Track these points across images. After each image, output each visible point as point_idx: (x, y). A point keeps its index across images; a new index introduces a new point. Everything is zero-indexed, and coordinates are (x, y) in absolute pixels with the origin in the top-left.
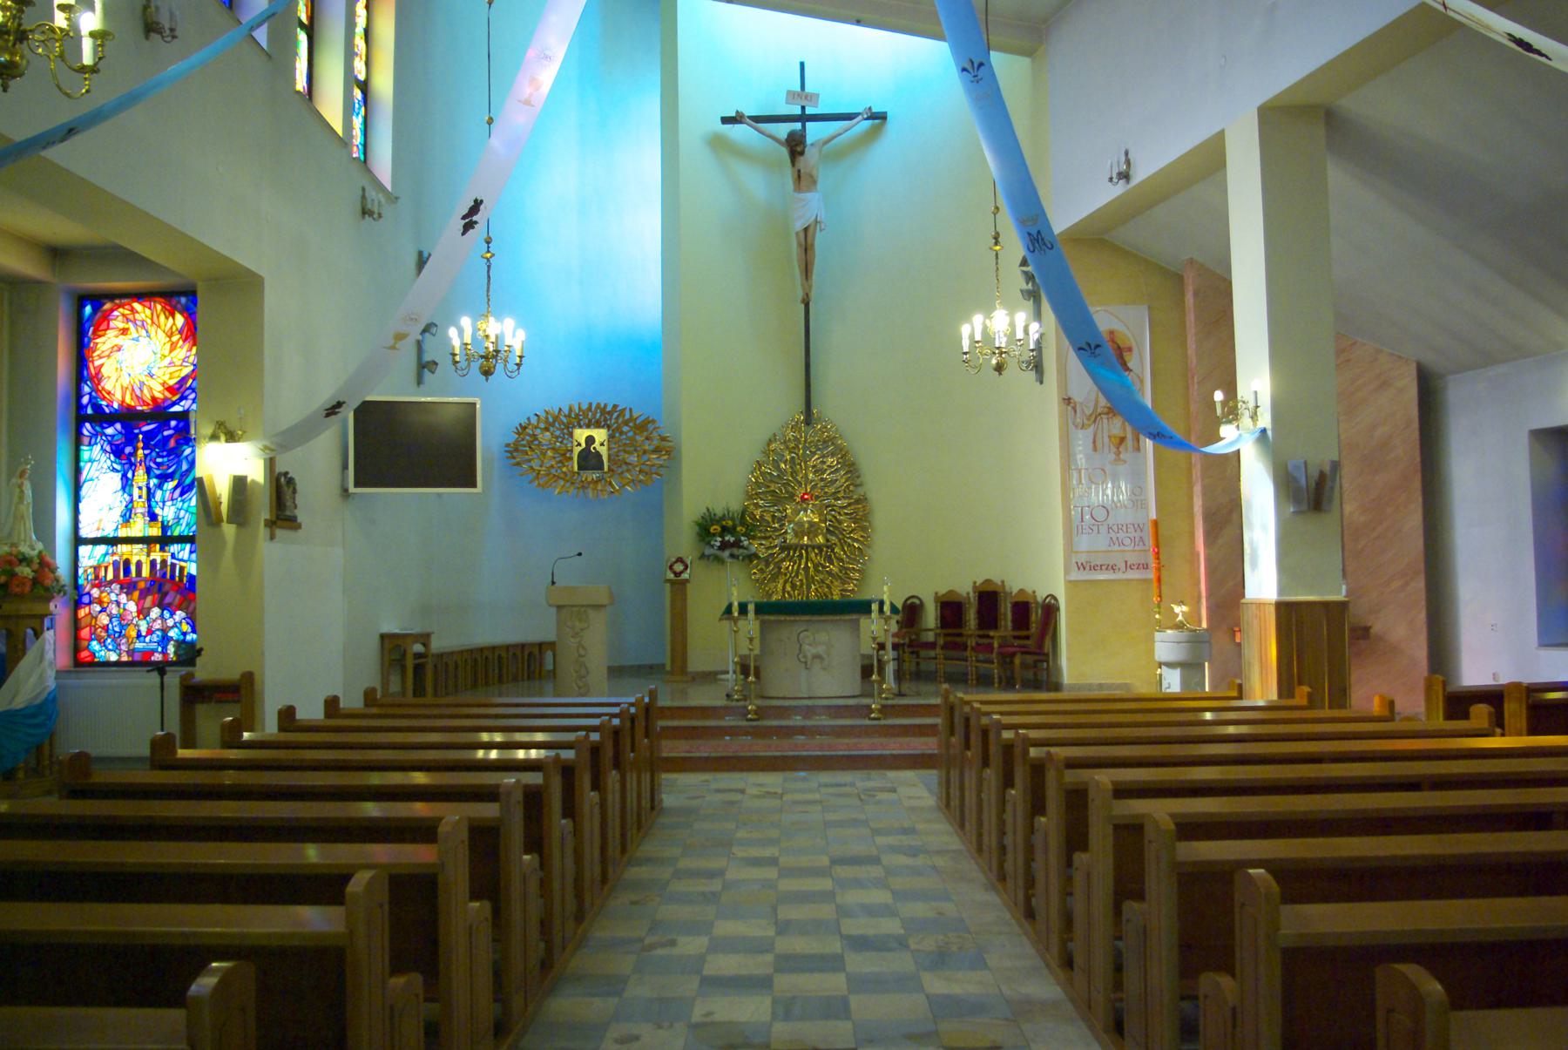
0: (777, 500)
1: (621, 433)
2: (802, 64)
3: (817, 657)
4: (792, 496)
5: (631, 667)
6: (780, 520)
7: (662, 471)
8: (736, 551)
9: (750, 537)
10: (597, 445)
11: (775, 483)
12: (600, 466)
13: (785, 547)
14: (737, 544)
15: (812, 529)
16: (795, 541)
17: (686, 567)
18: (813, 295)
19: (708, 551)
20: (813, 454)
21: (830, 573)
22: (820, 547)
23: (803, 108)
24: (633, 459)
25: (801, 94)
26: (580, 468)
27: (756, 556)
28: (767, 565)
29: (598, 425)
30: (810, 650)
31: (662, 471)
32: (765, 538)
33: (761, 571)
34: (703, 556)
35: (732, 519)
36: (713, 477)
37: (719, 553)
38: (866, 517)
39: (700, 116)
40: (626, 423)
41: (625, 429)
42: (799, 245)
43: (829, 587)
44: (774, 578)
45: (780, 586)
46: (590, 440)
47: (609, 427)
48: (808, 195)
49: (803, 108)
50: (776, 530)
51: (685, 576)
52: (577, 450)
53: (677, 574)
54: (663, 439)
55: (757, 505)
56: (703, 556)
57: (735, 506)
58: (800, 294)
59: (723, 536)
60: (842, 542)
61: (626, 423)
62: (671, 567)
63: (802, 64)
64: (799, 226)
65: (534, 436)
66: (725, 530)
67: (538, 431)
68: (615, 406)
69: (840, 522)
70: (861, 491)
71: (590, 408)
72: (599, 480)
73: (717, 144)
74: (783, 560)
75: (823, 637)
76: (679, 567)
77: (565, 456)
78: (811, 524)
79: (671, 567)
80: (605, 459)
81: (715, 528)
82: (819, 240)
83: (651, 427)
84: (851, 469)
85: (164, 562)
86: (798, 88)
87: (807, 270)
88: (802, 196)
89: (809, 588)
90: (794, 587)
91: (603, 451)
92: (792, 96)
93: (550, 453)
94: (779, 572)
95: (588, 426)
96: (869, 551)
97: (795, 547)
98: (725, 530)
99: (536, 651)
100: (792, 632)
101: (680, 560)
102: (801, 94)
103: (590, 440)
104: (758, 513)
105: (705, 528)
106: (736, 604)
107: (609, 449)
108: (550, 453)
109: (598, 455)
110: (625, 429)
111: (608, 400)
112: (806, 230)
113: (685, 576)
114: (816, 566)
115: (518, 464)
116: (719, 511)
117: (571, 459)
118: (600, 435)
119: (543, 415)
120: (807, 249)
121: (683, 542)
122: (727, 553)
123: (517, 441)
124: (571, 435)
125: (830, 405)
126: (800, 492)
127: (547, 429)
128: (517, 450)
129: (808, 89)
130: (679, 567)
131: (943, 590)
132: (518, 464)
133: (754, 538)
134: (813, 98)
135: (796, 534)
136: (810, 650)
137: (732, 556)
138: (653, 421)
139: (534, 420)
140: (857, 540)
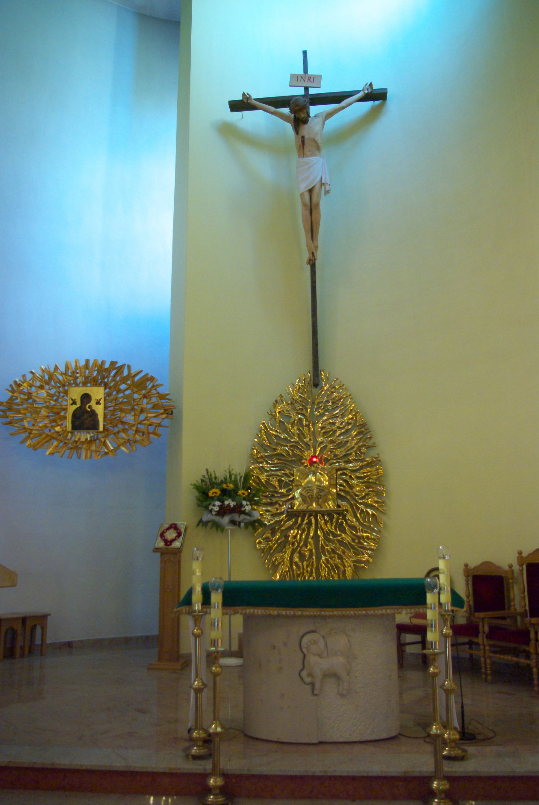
0: (285, 462)
1: (119, 391)
2: (305, 53)
3: (332, 675)
4: (300, 460)
5: (138, 638)
6: (287, 485)
7: (160, 430)
8: (236, 517)
9: (250, 499)
10: (93, 403)
11: (281, 448)
12: (94, 426)
13: (292, 514)
14: (238, 509)
15: (321, 494)
16: (304, 507)
17: (179, 535)
18: (319, 256)
19: (207, 517)
20: (323, 415)
21: (341, 543)
22: (330, 514)
23: (306, 89)
24: (130, 418)
25: (305, 78)
26: (74, 427)
27: (260, 523)
28: (273, 533)
29: (95, 383)
30: (319, 664)
31: (160, 430)
32: (271, 504)
33: (267, 539)
34: (201, 523)
35: (235, 483)
36: (218, 437)
37: (217, 519)
38: (380, 480)
39: (211, 99)
40: (124, 380)
41: (123, 387)
42: (304, 205)
43: (340, 558)
44: (282, 546)
45: (287, 556)
46: (86, 398)
47: (106, 385)
48: (313, 159)
49: (306, 89)
50: (283, 495)
51: (177, 544)
52: (72, 409)
53: (168, 543)
54: (162, 397)
55: (262, 469)
56: (201, 523)
57: (239, 470)
58: (306, 256)
59: (225, 501)
60: (355, 509)
61: (124, 380)
62: (162, 535)
63: (305, 53)
64: (304, 187)
65: (30, 394)
66: (225, 493)
67: (33, 389)
68: (113, 363)
69: (351, 487)
70: (373, 453)
71: (87, 366)
72: (92, 441)
73: (227, 131)
74: (291, 528)
75: (340, 642)
76: (171, 535)
77: (57, 415)
78: (321, 489)
79: (162, 535)
80: (101, 418)
81: (214, 492)
82: (326, 206)
83: (149, 385)
84: (364, 430)
85: (331, 548)
86: (301, 72)
87: (312, 231)
88: (306, 159)
89: (319, 558)
90: (302, 557)
91: (100, 410)
92: (295, 80)
93: (44, 412)
94: (286, 542)
95: (85, 384)
96: (384, 518)
97: (302, 514)
98: (225, 493)
99: (18, 627)
100: (288, 635)
101: (174, 526)
102: (305, 78)
103: (86, 398)
104: (263, 478)
105: (203, 493)
106: (198, 589)
107: (105, 408)
108: (44, 412)
109: (93, 414)
110: (123, 387)
111: (106, 357)
112: (311, 191)
113: (177, 544)
114: (326, 534)
115: (10, 423)
116: (220, 474)
117: (65, 418)
118: (98, 393)
119: (38, 373)
120: (312, 209)
121: (183, 508)
122: (226, 520)
123: (11, 398)
124: (66, 393)
125: (335, 367)
126: (308, 454)
127: (42, 387)
128: (10, 409)
129: (310, 72)
130: (171, 535)
131: (474, 562)
132: (10, 423)
133: (257, 503)
134: (316, 79)
135: (304, 499)
136: (319, 664)
137: (233, 522)
138: (152, 379)
139: (29, 377)
140: (371, 506)
